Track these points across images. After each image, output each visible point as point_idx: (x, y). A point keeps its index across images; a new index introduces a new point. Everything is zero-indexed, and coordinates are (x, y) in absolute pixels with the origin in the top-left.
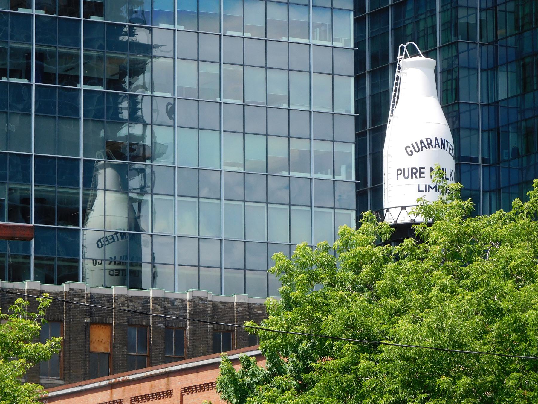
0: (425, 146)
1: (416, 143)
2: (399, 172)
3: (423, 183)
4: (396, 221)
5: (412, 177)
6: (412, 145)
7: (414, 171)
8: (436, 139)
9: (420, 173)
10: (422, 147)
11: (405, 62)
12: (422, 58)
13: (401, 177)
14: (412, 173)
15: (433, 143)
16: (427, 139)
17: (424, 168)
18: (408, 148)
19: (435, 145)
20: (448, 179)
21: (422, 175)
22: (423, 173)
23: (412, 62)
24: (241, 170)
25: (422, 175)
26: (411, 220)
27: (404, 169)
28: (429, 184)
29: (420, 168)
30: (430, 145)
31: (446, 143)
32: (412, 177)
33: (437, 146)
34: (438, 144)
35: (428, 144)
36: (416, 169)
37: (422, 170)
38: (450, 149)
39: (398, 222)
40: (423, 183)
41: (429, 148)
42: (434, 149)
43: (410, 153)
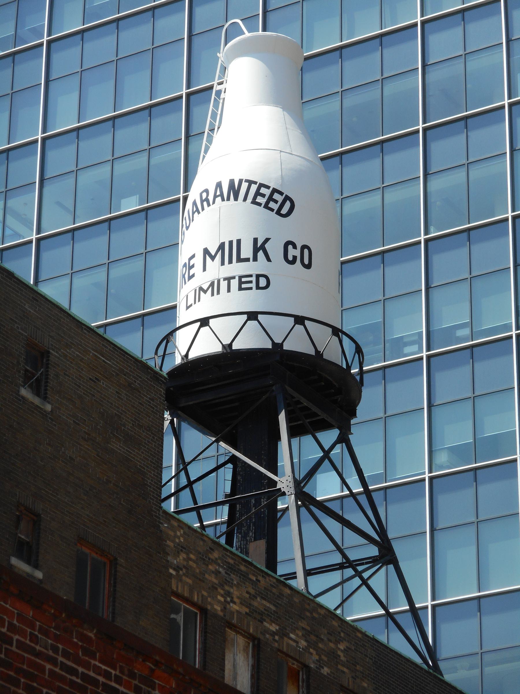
39: (286, 347)
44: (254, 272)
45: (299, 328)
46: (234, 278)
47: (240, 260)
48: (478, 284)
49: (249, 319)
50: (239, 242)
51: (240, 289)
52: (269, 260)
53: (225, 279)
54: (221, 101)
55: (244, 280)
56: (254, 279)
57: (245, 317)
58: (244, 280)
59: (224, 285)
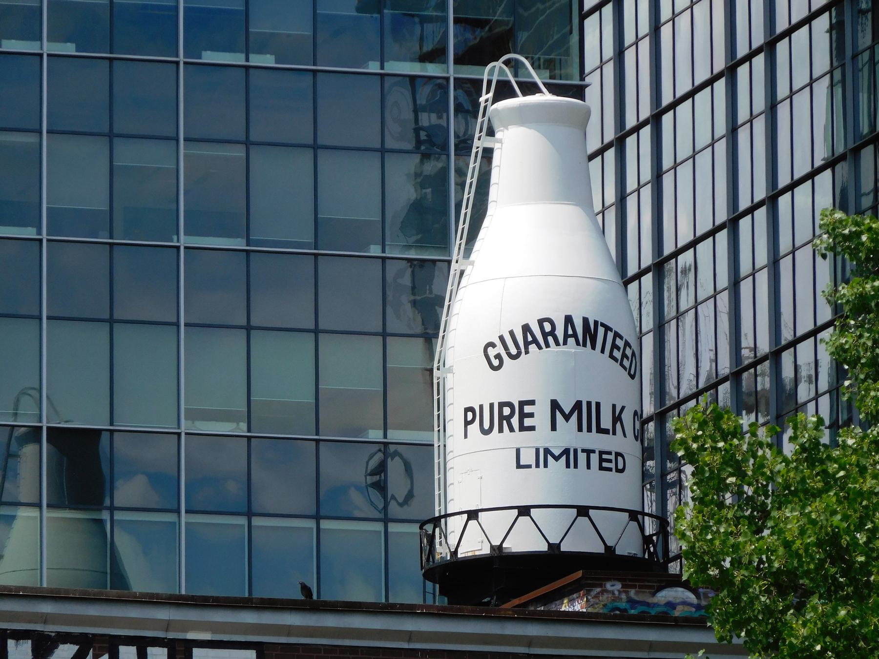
0: (535, 341)
1: (512, 333)
2: (470, 415)
3: (528, 443)
4: (455, 552)
5: (501, 430)
6: (501, 338)
7: (507, 411)
8: (569, 320)
9: (523, 416)
10: (527, 344)
11: (496, 110)
12: (546, 97)
13: (474, 428)
14: (502, 418)
15: (560, 333)
16: (541, 322)
17: (532, 403)
18: (490, 349)
19: (566, 336)
20: (606, 432)
21: (528, 422)
22: (531, 415)
23: (521, 108)
24: (242, 428)
25: (528, 422)
26: (550, 545)
27: (481, 407)
28: (547, 445)
29: (522, 404)
30: (550, 339)
31: (601, 330)
32: (501, 430)
33: (571, 341)
34: (575, 335)
35: (545, 335)
36: (510, 405)
37: (527, 409)
38: (614, 346)
39: (564, 548)
40: (528, 443)
41: (547, 346)
42: (562, 348)
43: (496, 363)
44: (614, 449)
45: (583, 520)
46: (594, 451)
47: (600, 430)
48: (255, 508)
49: (468, 519)
50: (598, 405)
51: (601, 468)
52: (625, 436)
53: (583, 451)
54: (474, 165)
55: (604, 456)
56: (612, 457)
57: (465, 516)
58: (604, 456)
59: (582, 457)
